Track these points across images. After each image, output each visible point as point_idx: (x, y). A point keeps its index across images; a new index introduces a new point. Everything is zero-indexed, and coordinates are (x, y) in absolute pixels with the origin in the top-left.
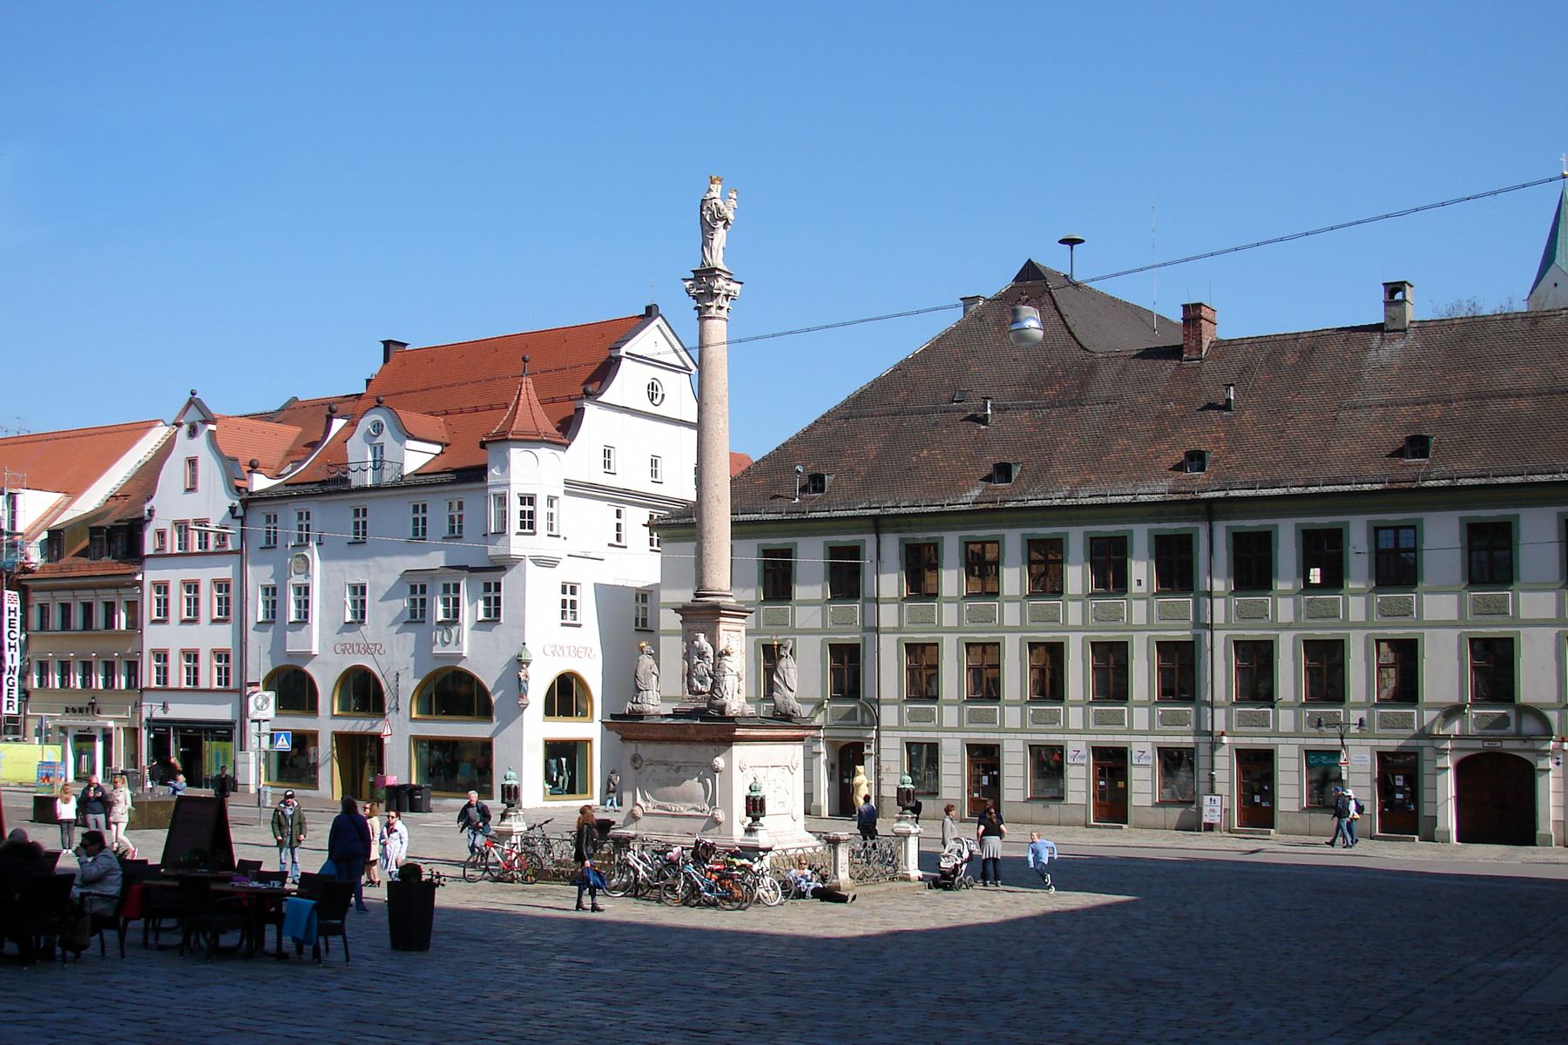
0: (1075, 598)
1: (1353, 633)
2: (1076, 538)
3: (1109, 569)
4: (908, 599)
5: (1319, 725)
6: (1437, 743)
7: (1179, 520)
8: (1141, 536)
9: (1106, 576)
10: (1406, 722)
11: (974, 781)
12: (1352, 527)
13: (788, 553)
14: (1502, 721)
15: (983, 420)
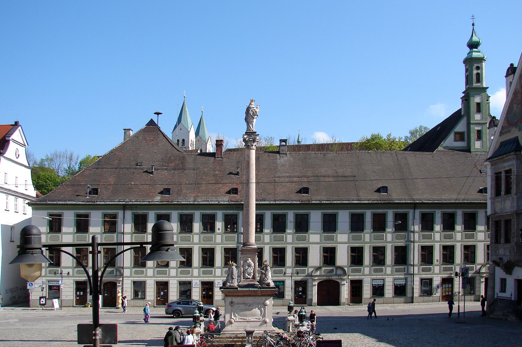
0: (196, 234)
1: (388, 244)
2: (197, 215)
3: (209, 225)
4: (134, 233)
5: (55, 274)
6: (313, 278)
7: (233, 210)
8: (220, 214)
9: (207, 227)
10: (451, 269)
11: (158, 293)
12: (172, 214)
13: (87, 216)
14: (332, 271)
15: (152, 173)
